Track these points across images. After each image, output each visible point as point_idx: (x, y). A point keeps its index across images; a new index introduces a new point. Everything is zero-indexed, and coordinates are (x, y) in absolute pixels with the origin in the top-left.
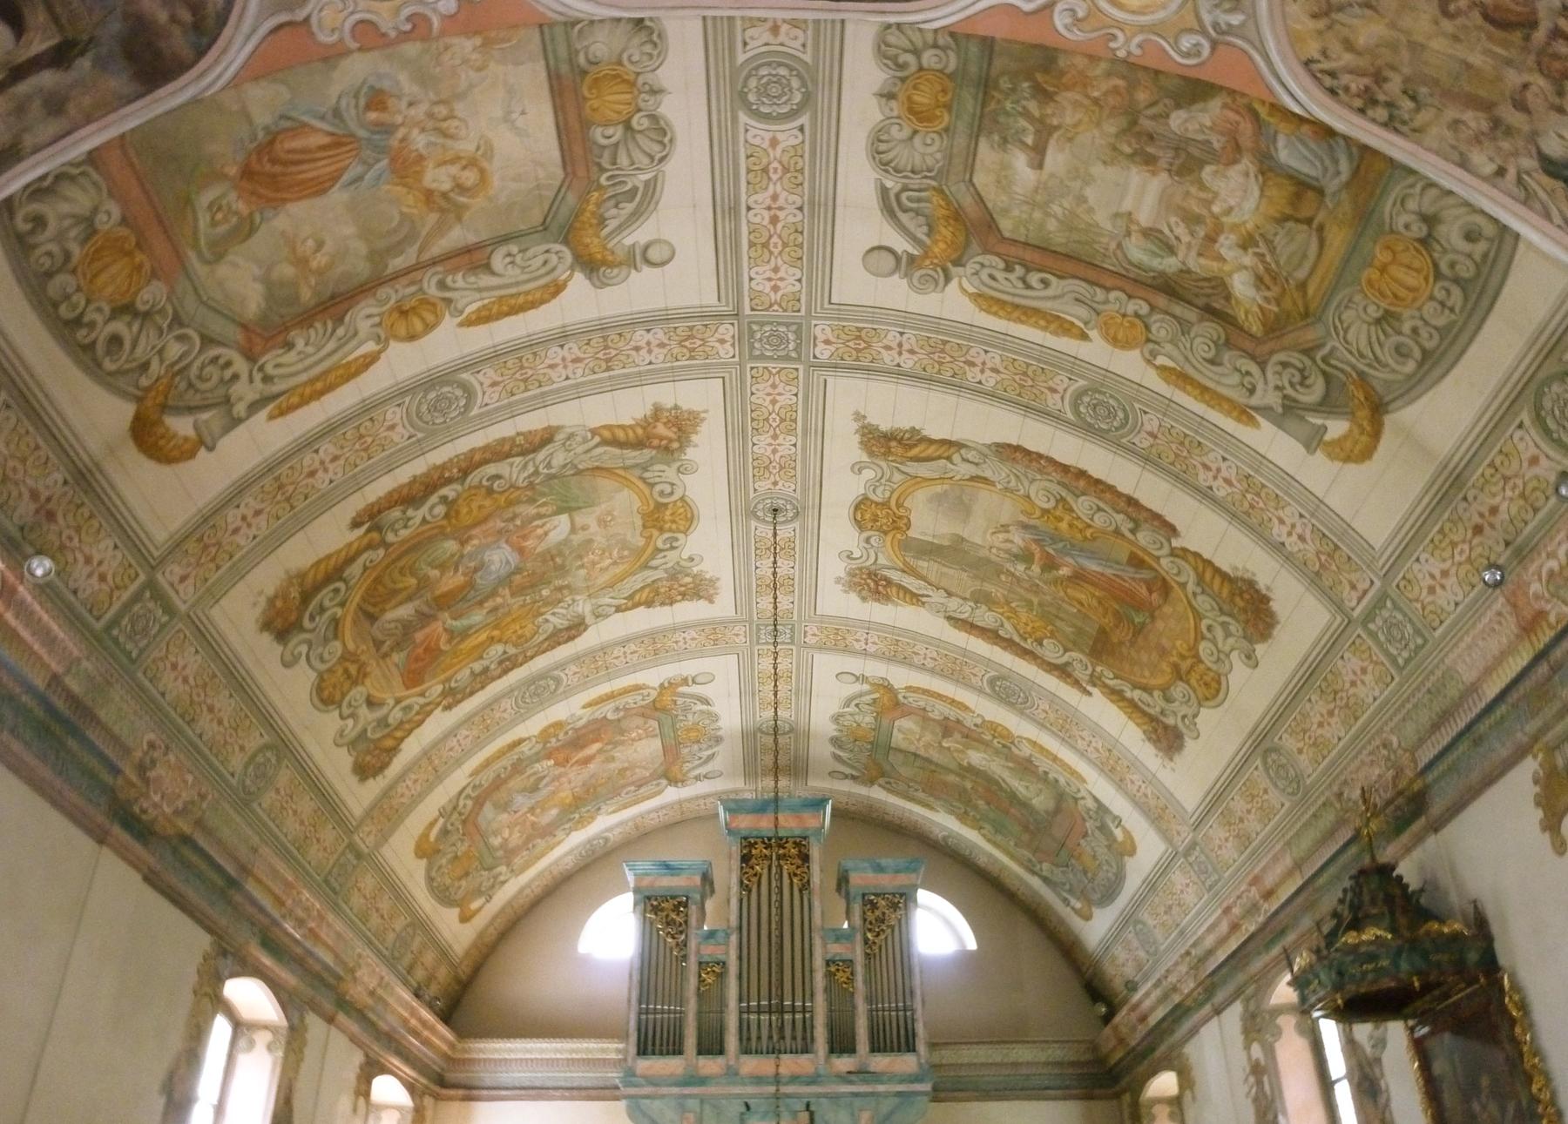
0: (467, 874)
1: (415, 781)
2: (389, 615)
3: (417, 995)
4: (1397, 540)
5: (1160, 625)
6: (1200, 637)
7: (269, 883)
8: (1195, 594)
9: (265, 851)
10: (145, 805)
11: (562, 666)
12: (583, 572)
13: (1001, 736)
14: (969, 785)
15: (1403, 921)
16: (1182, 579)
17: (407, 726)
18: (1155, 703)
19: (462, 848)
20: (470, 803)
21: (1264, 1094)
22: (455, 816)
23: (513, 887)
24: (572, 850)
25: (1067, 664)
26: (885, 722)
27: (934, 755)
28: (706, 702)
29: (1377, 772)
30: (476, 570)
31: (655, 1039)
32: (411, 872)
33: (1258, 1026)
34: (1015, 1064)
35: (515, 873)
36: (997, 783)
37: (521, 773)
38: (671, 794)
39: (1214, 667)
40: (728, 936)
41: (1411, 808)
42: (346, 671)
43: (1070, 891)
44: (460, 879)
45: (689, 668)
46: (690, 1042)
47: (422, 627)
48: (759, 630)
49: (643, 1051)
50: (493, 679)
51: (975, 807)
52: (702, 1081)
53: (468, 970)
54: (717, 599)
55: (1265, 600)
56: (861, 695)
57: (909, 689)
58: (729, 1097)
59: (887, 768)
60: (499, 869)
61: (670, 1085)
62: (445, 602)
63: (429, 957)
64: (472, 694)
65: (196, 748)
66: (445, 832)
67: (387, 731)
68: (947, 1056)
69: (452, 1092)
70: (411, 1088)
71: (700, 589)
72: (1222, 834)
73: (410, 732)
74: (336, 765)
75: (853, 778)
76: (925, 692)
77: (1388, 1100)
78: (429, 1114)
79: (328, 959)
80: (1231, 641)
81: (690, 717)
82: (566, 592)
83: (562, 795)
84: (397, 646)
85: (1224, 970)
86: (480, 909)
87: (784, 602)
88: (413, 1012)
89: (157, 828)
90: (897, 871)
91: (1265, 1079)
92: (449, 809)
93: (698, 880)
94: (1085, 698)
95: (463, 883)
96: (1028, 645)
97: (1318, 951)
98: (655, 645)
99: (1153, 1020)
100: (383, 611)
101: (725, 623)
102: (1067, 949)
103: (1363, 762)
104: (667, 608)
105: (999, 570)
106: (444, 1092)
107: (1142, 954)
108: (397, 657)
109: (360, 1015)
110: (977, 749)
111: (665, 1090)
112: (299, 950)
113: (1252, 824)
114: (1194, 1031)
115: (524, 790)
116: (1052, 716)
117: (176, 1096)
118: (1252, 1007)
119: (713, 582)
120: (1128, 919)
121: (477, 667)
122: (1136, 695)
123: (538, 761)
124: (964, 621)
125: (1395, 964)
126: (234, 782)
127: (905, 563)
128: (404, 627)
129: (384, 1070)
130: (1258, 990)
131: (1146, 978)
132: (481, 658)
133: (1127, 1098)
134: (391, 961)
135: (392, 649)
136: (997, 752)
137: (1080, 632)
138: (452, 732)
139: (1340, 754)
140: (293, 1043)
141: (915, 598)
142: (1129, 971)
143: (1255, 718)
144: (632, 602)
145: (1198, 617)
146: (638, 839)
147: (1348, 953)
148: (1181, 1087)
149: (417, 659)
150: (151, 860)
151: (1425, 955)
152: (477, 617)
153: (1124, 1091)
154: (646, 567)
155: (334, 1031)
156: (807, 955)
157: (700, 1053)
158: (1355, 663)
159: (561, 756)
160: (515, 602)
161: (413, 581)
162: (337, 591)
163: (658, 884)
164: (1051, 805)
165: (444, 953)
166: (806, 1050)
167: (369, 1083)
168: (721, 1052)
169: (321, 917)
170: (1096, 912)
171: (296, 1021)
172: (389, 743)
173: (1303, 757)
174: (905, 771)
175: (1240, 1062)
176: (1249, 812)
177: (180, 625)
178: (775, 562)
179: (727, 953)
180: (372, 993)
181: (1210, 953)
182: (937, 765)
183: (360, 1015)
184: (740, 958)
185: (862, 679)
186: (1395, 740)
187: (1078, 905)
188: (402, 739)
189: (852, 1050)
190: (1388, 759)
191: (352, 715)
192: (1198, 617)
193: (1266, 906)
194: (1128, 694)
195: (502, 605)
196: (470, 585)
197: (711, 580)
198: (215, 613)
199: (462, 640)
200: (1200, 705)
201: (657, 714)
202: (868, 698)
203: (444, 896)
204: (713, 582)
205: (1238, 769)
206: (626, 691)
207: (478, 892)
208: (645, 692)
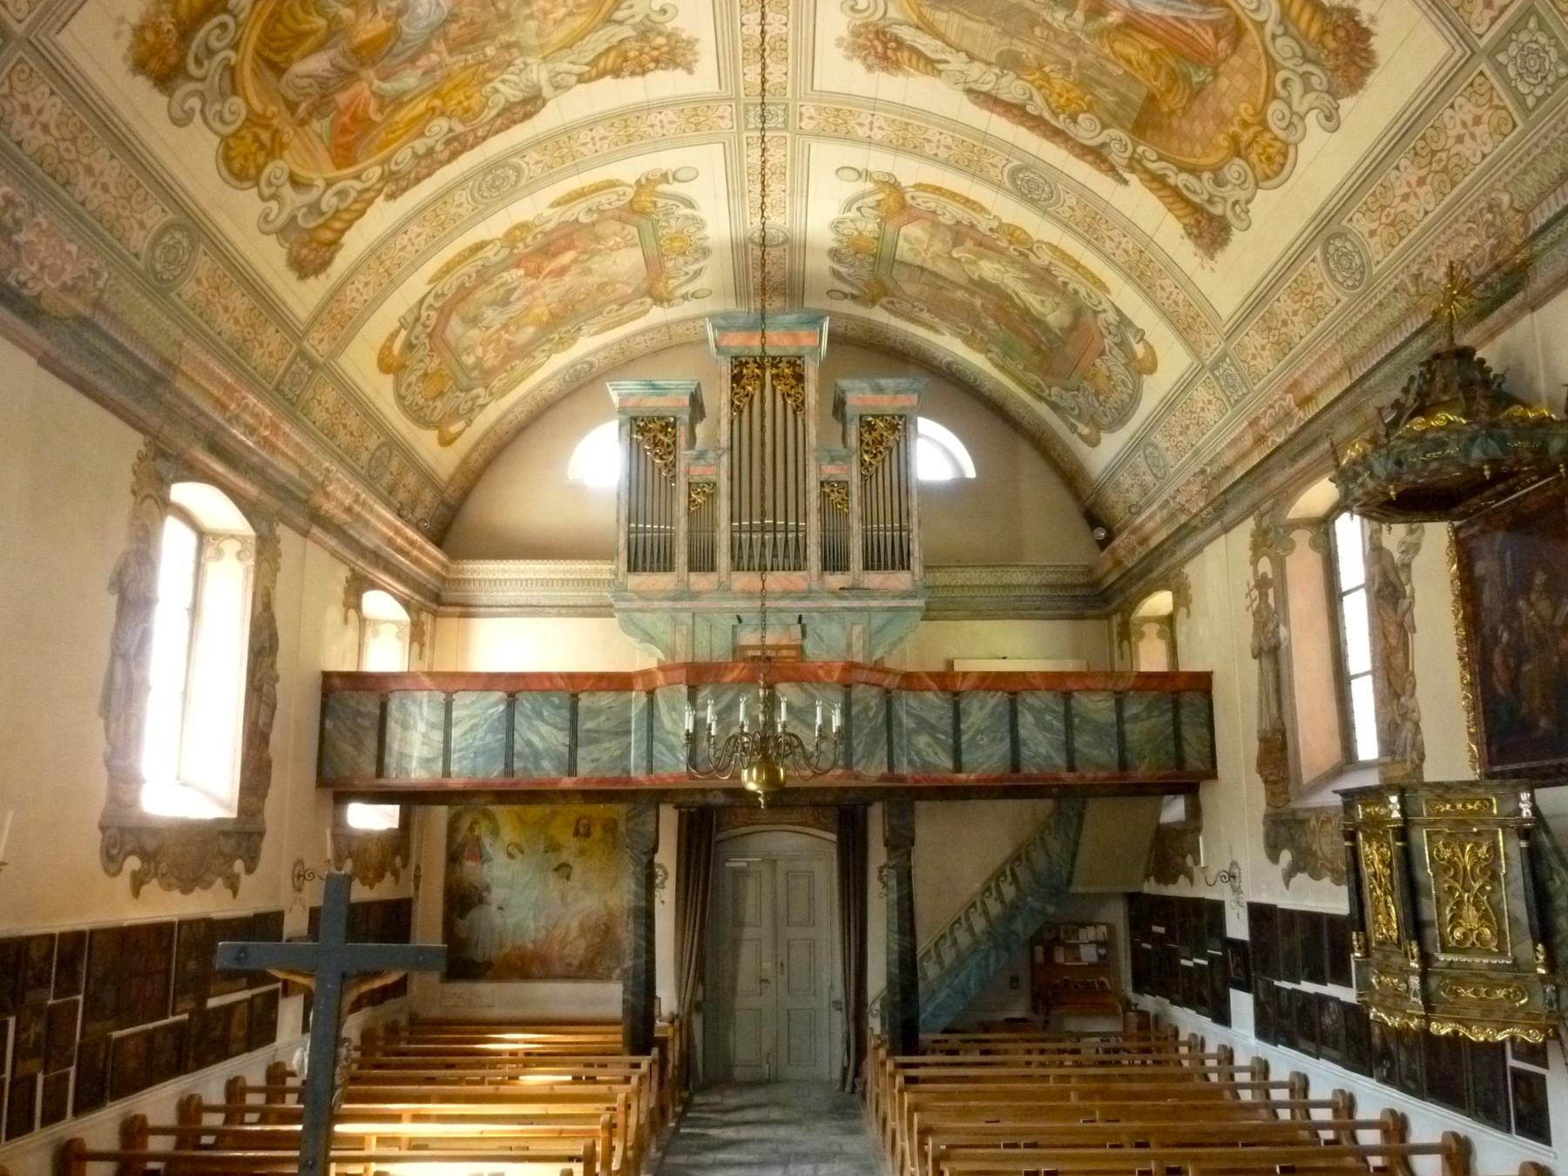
0: (441, 394)
1: (366, 284)
2: (299, 68)
3: (400, 516)
4: (1442, 73)
5: (1224, 83)
6: (1271, 95)
7: (203, 382)
8: (1274, 37)
9: (188, 344)
10: (22, 278)
11: (520, 151)
12: (532, 25)
13: (1020, 242)
14: (978, 302)
15: (1483, 404)
16: (1259, 17)
17: (346, 216)
18: (1200, 188)
19: (434, 365)
20: (434, 314)
21: (1268, 606)
22: (419, 328)
23: (494, 412)
24: (554, 375)
25: (1104, 145)
26: (890, 229)
27: (942, 268)
28: (690, 204)
29: (1474, 241)
30: (400, 13)
31: (646, 555)
32: (381, 391)
33: (1271, 540)
34: (1009, 586)
35: (496, 395)
36: (1009, 298)
37: (487, 282)
38: (657, 315)
39: (1281, 135)
40: (719, 457)
41: (1506, 284)
42: (256, 139)
43: (1079, 417)
44: (434, 399)
45: (667, 160)
46: (681, 559)
47: (344, 88)
48: (747, 111)
49: (633, 567)
50: (442, 164)
51: (984, 328)
52: (694, 596)
53: (456, 495)
54: (697, 68)
55: (1366, 34)
56: (863, 196)
57: (918, 186)
58: (721, 611)
59: (890, 285)
60: (475, 392)
61: (663, 599)
62: (369, 54)
63: (411, 480)
64: (418, 180)
65: (80, 218)
66: (409, 346)
67: (321, 220)
68: (942, 578)
69: (450, 609)
70: (406, 604)
71: (675, 55)
72: (1259, 341)
73: (350, 223)
74: (268, 258)
75: (854, 297)
76: (937, 190)
77: (1411, 604)
78: (428, 628)
79: (293, 472)
80: (1311, 97)
81: (673, 222)
82: (514, 51)
83: (537, 311)
84: (317, 111)
85: (1241, 487)
86: (460, 434)
87: (775, 74)
88: (398, 531)
89: (44, 304)
90: (898, 392)
91: (1271, 592)
92: (410, 319)
93: (686, 400)
94: (1120, 188)
95: (438, 404)
96: (1061, 123)
97: (1374, 440)
98: (626, 128)
99: (1153, 543)
100: (290, 61)
101: (708, 102)
102: (1070, 476)
103: (1458, 233)
104: (638, 80)
105: (1033, 21)
106: (442, 609)
107: (1149, 478)
108: (319, 126)
109: (338, 531)
110: (989, 258)
111: (656, 604)
112: (255, 459)
113: (1297, 327)
114: (1198, 550)
115: (493, 303)
116: (1079, 213)
117: (130, 595)
118: (1266, 522)
119: (691, 43)
120: (1140, 442)
121: (420, 146)
122: (1180, 180)
123: (506, 269)
124: (987, 94)
125: (1466, 452)
126: (140, 265)
127: (921, 16)
128: (320, 84)
129: (374, 586)
130: (1276, 504)
131: (1150, 503)
132: (422, 135)
133: (1117, 618)
134: (369, 481)
135: (310, 114)
136: (1013, 262)
137: (1124, 101)
138: (400, 229)
139: (1424, 232)
140: (266, 551)
141: (930, 65)
142: (1134, 496)
143: (1322, 198)
144: (597, 71)
145: (1273, 66)
146: (623, 362)
147: (1411, 441)
148: (1176, 605)
149: (344, 131)
150: (46, 344)
151: (1502, 442)
152: (410, 80)
153: (1116, 611)
154: (609, 21)
155: (309, 543)
156: (801, 477)
157: (691, 569)
158: (1467, 110)
159: (532, 266)
160: (456, 62)
161: (321, 23)
162: (223, 26)
163: (643, 404)
164: (1067, 321)
165: (427, 477)
166: (798, 568)
167: (359, 597)
168: (713, 569)
169: (275, 428)
170: (1104, 436)
171: (266, 532)
172: (328, 235)
173: (1373, 241)
174: (910, 289)
175: (1245, 575)
176: (1295, 313)
177: (20, 53)
178: (763, 18)
179: (718, 474)
180: (349, 510)
181: (1228, 469)
182: (945, 279)
183: (338, 531)
184: (731, 478)
185: (865, 175)
186: (1506, 199)
187: (1086, 431)
188: (342, 232)
189: (845, 568)
190: (1492, 224)
191: (274, 197)
192: (1273, 66)
193: (1301, 414)
194: (1172, 181)
195: (441, 65)
196: (394, 33)
197: (689, 42)
198: (63, 39)
199: (394, 111)
200: (1257, 186)
201: (636, 218)
202: (871, 200)
203: (418, 416)
204: (691, 43)
205: (1294, 259)
206: (598, 188)
207: (456, 415)
208: (620, 190)
